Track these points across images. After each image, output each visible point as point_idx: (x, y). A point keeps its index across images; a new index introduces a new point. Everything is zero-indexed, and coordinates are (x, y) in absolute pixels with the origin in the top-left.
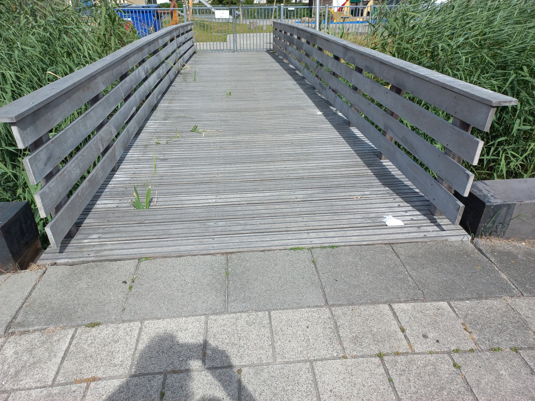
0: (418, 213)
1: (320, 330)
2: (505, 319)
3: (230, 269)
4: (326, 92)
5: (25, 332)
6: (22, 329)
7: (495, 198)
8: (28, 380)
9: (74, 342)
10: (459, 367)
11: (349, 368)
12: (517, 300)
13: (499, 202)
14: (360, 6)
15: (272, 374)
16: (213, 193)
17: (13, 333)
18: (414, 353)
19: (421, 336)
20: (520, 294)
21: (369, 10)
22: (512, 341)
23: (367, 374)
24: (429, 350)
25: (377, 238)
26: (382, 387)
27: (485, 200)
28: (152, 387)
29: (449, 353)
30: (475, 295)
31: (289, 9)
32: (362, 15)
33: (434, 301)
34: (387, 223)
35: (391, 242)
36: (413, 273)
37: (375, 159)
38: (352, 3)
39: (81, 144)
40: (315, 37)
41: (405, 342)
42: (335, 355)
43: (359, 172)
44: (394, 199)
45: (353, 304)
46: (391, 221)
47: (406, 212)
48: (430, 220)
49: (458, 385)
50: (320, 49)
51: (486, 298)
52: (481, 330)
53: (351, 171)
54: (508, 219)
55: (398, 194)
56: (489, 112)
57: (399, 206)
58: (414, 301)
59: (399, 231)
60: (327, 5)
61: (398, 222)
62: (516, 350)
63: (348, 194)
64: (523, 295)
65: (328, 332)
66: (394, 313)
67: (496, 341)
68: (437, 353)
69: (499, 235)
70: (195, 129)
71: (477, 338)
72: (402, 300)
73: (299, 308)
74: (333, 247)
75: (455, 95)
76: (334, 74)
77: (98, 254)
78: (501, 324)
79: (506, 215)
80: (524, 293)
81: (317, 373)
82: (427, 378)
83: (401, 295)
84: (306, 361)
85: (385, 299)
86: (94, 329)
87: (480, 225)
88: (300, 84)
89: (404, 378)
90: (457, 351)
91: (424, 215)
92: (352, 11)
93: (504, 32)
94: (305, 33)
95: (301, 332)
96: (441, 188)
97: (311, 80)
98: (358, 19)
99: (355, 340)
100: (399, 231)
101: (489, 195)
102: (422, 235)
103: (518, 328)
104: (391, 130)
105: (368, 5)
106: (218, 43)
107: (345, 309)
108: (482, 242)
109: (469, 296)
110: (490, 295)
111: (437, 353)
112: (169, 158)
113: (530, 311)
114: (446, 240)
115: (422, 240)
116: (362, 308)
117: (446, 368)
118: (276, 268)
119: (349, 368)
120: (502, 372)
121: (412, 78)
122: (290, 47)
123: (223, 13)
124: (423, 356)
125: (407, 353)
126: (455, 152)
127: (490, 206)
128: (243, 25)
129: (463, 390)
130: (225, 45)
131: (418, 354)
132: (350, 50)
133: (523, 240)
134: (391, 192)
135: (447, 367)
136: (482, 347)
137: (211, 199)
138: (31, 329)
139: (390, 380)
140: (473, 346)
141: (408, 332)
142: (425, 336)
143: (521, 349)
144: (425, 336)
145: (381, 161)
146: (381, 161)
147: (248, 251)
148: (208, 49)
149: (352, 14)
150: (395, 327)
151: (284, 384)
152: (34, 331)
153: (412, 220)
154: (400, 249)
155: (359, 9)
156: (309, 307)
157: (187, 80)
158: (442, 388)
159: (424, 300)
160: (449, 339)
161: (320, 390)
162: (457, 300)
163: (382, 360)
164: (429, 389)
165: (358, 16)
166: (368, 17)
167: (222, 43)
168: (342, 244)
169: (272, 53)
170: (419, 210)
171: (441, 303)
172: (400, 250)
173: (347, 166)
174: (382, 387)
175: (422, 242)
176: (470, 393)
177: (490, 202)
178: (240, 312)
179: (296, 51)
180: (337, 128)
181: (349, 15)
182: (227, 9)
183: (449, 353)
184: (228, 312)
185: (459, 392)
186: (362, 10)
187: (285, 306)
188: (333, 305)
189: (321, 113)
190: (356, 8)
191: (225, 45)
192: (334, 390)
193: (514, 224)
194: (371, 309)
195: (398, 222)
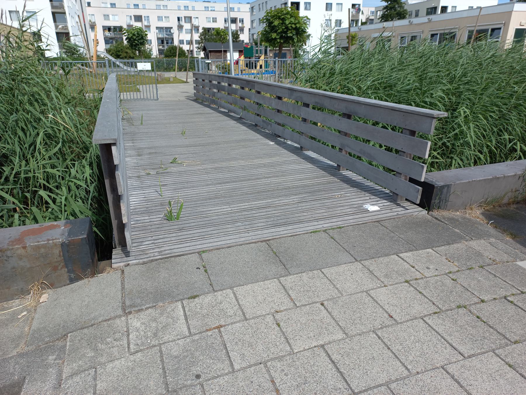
0: (386, 201)
1: (361, 275)
2: (468, 253)
3: (274, 250)
4: (271, 127)
5: (139, 311)
6: (136, 309)
7: (439, 182)
8: (168, 336)
9: (187, 309)
10: (455, 280)
11: (392, 291)
12: (470, 242)
13: (442, 184)
14: (253, 59)
15: (345, 302)
16: (228, 204)
17: (130, 313)
18: (426, 277)
19: (425, 268)
20: (470, 239)
21: (261, 64)
22: (477, 263)
23: (405, 292)
24: (434, 274)
25: (367, 219)
26: (417, 297)
27: (433, 184)
28: (268, 322)
29: (446, 274)
30: (445, 243)
31: (206, 62)
32: (256, 68)
33: (423, 249)
34: (369, 209)
35: (377, 220)
36: (402, 236)
37: (335, 171)
38: (245, 57)
39: (311, 121)
40: (252, 83)
41: (418, 273)
42: (379, 286)
43: (329, 180)
44: (364, 194)
45: (373, 258)
46: (372, 208)
47: (377, 201)
48: (396, 204)
49: (459, 289)
50: (259, 93)
51: (453, 244)
52: (458, 260)
53: (322, 180)
54: (448, 195)
55: (365, 191)
56: (432, 122)
57: (370, 199)
58: (412, 251)
59: (378, 213)
60: (277, 58)
61: (376, 208)
62: (482, 267)
63: (330, 195)
64: (472, 239)
65: (367, 275)
66: (402, 259)
67: (468, 264)
68: (440, 275)
69: (445, 208)
70: (174, 161)
71: (458, 265)
72: (403, 251)
73: (339, 265)
74: (340, 228)
75: (404, 114)
76: (279, 111)
77: (161, 254)
78: (467, 256)
79: (447, 193)
80: (472, 238)
81: (374, 296)
82: (440, 288)
83: (401, 249)
84: (363, 292)
85: (393, 252)
86: (196, 299)
87: (432, 202)
88: (240, 123)
89: (427, 290)
90: (450, 272)
91: (390, 202)
92: (247, 64)
93: (393, 77)
94: (239, 81)
95: (349, 278)
96: (401, 180)
97: (252, 119)
98: (253, 72)
99: (386, 276)
100: (378, 213)
101: (434, 181)
102: (396, 213)
103: (478, 256)
104: (348, 146)
105: (260, 59)
106: (125, 93)
107: (370, 261)
108: (435, 213)
109: (443, 244)
110: (454, 242)
111: (440, 275)
112: (168, 184)
113: (480, 247)
114: (412, 215)
115: (397, 216)
116: (381, 259)
117: (448, 282)
118: (308, 245)
119: (392, 291)
120: (479, 278)
121: (364, 106)
122: (219, 94)
123: (145, 65)
124: (433, 278)
125: (422, 278)
126: (409, 152)
127: (437, 187)
128: (148, 77)
129: (463, 290)
130: (139, 95)
131: (429, 277)
132: (296, 91)
133: (457, 210)
134: (359, 190)
135: (448, 281)
136: (463, 268)
137: (227, 209)
138: (144, 308)
139: (420, 293)
140: (457, 269)
141: (416, 267)
142: (428, 268)
143: (484, 266)
144: (428, 268)
145: (340, 172)
146: (340, 172)
147: (280, 238)
148: (132, 98)
149: (247, 66)
150: (407, 266)
151: (356, 306)
152: (147, 308)
153: (384, 206)
154: (386, 224)
155: (252, 63)
156: (345, 263)
157: (134, 124)
158: (452, 292)
159: (417, 250)
160: (442, 267)
161: (381, 304)
162: (436, 247)
163: (410, 284)
164: (445, 293)
165: (252, 68)
166: (261, 69)
167: (135, 93)
168: (346, 225)
169: (197, 99)
170: (386, 200)
171: (428, 250)
172: (386, 224)
173: (317, 178)
174: (417, 297)
175: (397, 218)
176: (467, 291)
177: (437, 184)
178: (299, 273)
179: (228, 96)
180: (293, 153)
181: (244, 68)
182: (148, 62)
183: (446, 274)
184: (290, 274)
185: (462, 292)
186: (256, 64)
187: (329, 265)
188: (361, 260)
189: (273, 143)
190: (250, 61)
191: (139, 95)
192: (390, 303)
193: (452, 198)
194: (386, 259)
195: (376, 208)
